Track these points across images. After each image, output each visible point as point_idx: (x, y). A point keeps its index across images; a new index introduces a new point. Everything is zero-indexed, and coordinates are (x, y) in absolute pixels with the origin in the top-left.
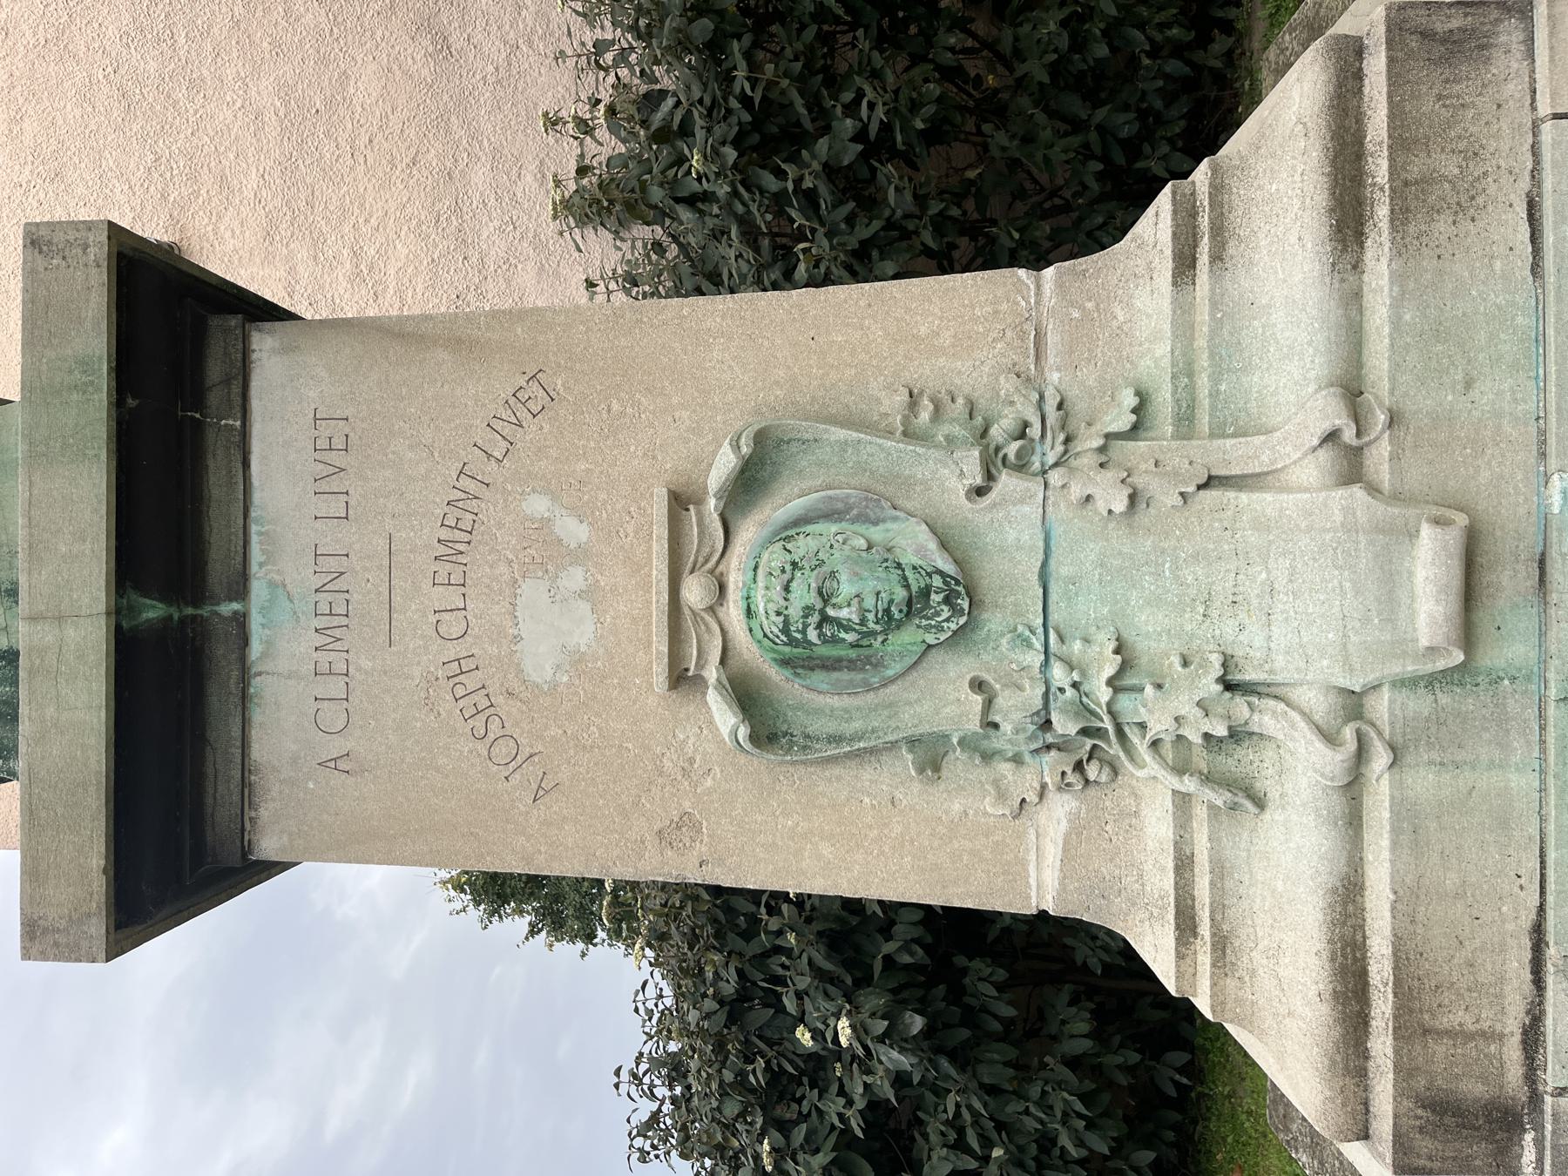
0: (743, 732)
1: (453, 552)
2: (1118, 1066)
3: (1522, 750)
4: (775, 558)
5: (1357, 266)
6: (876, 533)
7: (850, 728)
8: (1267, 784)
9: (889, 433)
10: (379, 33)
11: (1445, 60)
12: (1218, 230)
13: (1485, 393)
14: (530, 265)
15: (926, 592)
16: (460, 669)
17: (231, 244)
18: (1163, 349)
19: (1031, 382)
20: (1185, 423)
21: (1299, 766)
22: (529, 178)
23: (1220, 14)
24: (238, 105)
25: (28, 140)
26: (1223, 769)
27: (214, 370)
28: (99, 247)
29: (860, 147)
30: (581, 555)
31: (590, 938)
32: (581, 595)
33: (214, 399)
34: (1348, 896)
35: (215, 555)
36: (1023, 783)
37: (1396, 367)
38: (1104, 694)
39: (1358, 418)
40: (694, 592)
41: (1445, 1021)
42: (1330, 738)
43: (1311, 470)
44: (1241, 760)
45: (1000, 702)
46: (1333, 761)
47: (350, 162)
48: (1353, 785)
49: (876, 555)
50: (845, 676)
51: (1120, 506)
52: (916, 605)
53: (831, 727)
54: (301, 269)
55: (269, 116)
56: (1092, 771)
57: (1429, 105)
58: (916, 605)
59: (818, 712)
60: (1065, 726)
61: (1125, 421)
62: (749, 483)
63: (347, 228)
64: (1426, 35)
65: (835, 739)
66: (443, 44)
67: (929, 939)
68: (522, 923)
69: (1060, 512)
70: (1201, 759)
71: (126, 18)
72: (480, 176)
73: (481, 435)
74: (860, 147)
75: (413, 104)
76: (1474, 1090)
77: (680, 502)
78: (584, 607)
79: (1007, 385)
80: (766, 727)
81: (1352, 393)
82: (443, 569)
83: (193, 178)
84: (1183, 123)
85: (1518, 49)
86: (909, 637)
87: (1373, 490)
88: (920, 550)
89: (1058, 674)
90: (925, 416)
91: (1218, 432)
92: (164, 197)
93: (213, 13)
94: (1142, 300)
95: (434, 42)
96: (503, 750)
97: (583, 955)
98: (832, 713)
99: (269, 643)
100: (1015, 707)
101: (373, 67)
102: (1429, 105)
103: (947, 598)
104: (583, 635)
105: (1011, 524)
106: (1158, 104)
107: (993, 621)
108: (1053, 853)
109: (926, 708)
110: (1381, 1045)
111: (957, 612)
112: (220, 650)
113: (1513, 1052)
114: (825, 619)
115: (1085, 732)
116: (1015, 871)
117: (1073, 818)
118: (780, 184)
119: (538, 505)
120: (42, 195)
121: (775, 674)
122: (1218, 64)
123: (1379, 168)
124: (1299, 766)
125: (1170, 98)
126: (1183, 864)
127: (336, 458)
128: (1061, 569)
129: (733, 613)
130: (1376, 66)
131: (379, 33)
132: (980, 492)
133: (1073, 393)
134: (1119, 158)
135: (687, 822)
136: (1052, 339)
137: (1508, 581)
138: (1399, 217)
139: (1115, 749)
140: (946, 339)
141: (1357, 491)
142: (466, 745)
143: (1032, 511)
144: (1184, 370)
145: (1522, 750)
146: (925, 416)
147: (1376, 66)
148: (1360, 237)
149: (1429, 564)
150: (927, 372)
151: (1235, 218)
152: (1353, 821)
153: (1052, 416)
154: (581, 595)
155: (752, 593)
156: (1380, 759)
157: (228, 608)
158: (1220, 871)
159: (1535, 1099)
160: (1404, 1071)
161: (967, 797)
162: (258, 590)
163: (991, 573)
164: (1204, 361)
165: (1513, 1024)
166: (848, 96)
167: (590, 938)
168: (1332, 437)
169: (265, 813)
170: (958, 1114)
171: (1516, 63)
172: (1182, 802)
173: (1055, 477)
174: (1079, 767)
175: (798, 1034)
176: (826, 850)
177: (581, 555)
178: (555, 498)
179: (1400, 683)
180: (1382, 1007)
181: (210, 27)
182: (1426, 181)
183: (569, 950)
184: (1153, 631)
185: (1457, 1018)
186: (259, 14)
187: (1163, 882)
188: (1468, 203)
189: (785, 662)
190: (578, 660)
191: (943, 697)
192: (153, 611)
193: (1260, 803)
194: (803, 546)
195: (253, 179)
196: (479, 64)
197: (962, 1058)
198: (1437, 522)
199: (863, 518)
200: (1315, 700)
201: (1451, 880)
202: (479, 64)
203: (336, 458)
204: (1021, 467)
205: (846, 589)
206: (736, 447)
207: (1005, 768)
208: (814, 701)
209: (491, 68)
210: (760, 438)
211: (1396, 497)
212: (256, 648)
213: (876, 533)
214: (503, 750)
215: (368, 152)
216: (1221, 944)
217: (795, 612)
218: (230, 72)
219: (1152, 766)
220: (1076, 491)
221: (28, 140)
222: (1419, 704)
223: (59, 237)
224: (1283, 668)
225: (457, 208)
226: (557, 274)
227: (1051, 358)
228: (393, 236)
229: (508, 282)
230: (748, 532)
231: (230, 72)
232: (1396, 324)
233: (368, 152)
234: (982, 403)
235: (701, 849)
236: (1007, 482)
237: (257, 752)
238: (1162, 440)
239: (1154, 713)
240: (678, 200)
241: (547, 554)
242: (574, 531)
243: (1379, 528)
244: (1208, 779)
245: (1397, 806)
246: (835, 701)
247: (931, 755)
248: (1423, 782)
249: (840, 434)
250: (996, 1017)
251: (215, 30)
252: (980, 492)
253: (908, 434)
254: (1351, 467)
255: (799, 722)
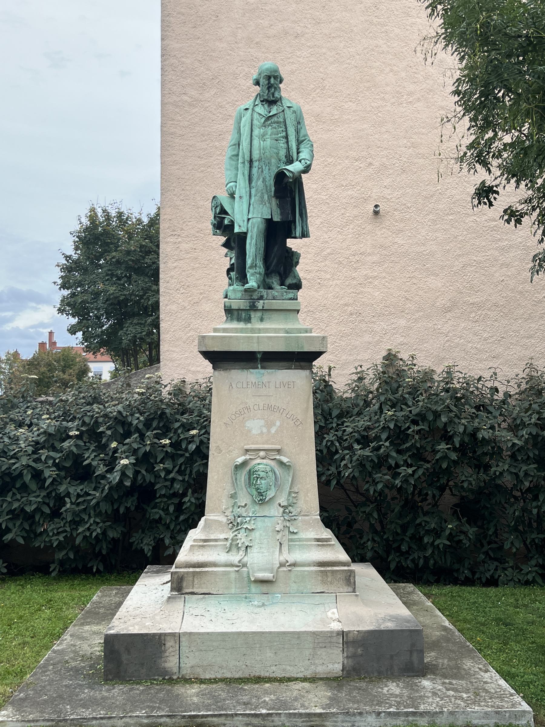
0: (238, 463)
1: (270, 408)
2: (102, 547)
3: (238, 591)
4: (268, 469)
5: (314, 566)
6: (273, 487)
7: (238, 481)
8: (230, 553)
9: (290, 489)
10: (451, 288)
11: (346, 579)
12: (323, 545)
13: (293, 585)
14: (371, 339)
15: (262, 496)
16: (248, 409)
17: (379, 233)
18: (304, 537)
19: (299, 514)
20: (290, 540)
21: (235, 557)
22: (401, 340)
23: (442, 579)
24: (428, 238)
25: (416, 161)
26: (233, 546)
27: (302, 364)
28: (322, 350)
29: (393, 465)
30: (269, 431)
31: (64, 286)
32: (262, 432)
33: (297, 363)
34: (214, 565)
35: (269, 364)
36: (228, 513)
37: (298, 571)
38: (245, 527)
39: (289, 566)
40: (262, 454)
41: (195, 579)
42: (239, 562)
43: (282, 559)
44: (234, 549)
45: (243, 509)
46: (236, 562)
47: (407, 276)
48: (232, 565)
49: (269, 487)
50: (248, 481)
51: (277, 529)
52: (260, 494)
53: (238, 478)
54: (370, 257)
55: (423, 248)
56: (231, 525)
57: (339, 576)
58: (260, 494)
59: (241, 476)
60: (239, 520)
61: (291, 530)
62: (281, 463)
63: (384, 274)
64: (350, 576)
65: (236, 479)
66: (448, 310)
67: (144, 485)
68: (70, 251)
69: (275, 519)
70: (234, 543)
71: (458, 197)
72: (402, 322)
73: (291, 413)
74: (393, 465)
75: (427, 299)
76: (184, 584)
77: (279, 451)
78: (259, 432)
79: (299, 510)
80: (238, 467)
81: (294, 565)
82: (267, 406)
83: (402, 220)
84: (406, 566)
85: (348, 591)
86: (255, 493)
87: (279, 568)
88: (270, 495)
89: (248, 519)
90: (293, 495)
91: (289, 546)
92: (395, 210)
93: (460, 229)
94: (313, 533)
95: (448, 307)
96: (233, 417)
97: (55, 283)
98: (241, 478)
99: (253, 373)
100: (242, 511)
101: (440, 285)
102: (339, 576)
103: (262, 499)
104: (254, 432)
105: (275, 511)
106: (411, 558)
107: (257, 507)
108: (216, 518)
109: (241, 495)
110: (191, 570)
111: (259, 501)
112: (252, 364)
113: (190, 590)
114: (258, 478)
115: (238, 523)
116: (212, 511)
117: (222, 522)
118: (384, 440)
119: (278, 423)
120: (397, 165)
121: (248, 468)
122: (425, 577)
123: (329, 568)
124: (235, 557)
125: (413, 561)
126: (216, 540)
127: (286, 386)
128: (266, 519)
129: (258, 461)
130: (346, 568)
131: (451, 288)
132: (280, 505)
133: (297, 521)
134: (395, 545)
135: (220, 451)
136: (307, 518)
137: (264, 588)
138: (322, 572)
139: (235, 529)
140: (307, 499)
141: (278, 565)
142: (234, 410)
143: (276, 514)
144: (300, 540)
145: (238, 591)
146: (293, 495)
147: (346, 568)
148: (319, 566)
149: (267, 575)
150: (301, 495)
151: (325, 548)
152: (226, 565)
153: (293, 518)
154: (262, 432)
155: (261, 464)
156: (237, 569)
157: (259, 366)
158: (216, 546)
159: (183, 594)
160: (188, 573)
161: (225, 503)
162: (263, 371)
163: (266, 507)
164: (301, 543)
165: (195, 590)
166: (409, 461)
167: (64, 286)
168: (287, 562)
169: (222, 372)
170: (90, 495)
171: (346, 590)
172: (226, 539)
173: (282, 518)
174: (231, 523)
175: (115, 442)
176: (216, 477)
177: (269, 431)
178: (279, 427)
179: (248, 572)
180: (198, 570)
181: (455, 228)
182: (327, 576)
183: (57, 275)
184: (256, 535)
185: (196, 581)
186: (459, 245)
187: (212, 537)
188: (324, 582)
189: (250, 470)
190: (249, 431)
191: (244, 499)
192: (259, 356)
193: (227, 552)
194: (270, 474)
195: (400, 242)
196: (441, 323)
197: (108, 498)
198: (274, 577)
199: (275, 484)
200: (245, 559)
201: (218, 580)
202: (441, 323)
203: (286, 386)
204: (284, 512)
205: (263, 482)
206: (288, 462)
207: (231, 510)
208: (243, 476)
209: (439, 327)
210: (290, 466)
211: (277, 571)
212: (252, 370)
213: (273, 487)
214: (233, 417)
215: (411, 283)
216: (203, 546)
217: (259, 473)
218: (439, 235)
219: (232, 535)
220: (280, 522)
221: (416, 161)
222: (245, 575)
223: (325, 342)
224: (250, 555)
225: (391, 314)
226: (368, 349)
227: (303, 518)
228: (382, 290)
229: (365, 331)
230: (273, 463)
231: (439, 235)
232: (305, 571)
233: (411, 283)
234: (295, 505)
235: (216, 454)
236: (282, 510)
237: (233, 371)
238: (288, 536)
239: (242, 535)
240: (381, 404)
241: (269, 425)
242: (273, 430)
243: (272, 569)
244: (231, 544)
245: (229, 572)
246: (243, 479)
247: (233, 496)
248: (233, 576)
249: (290, 480)
250: (119, 506)
251: (453, 230)
252: (280, 505)
253: (290, 493)
254: (282, 565)
255: (239, 472)
